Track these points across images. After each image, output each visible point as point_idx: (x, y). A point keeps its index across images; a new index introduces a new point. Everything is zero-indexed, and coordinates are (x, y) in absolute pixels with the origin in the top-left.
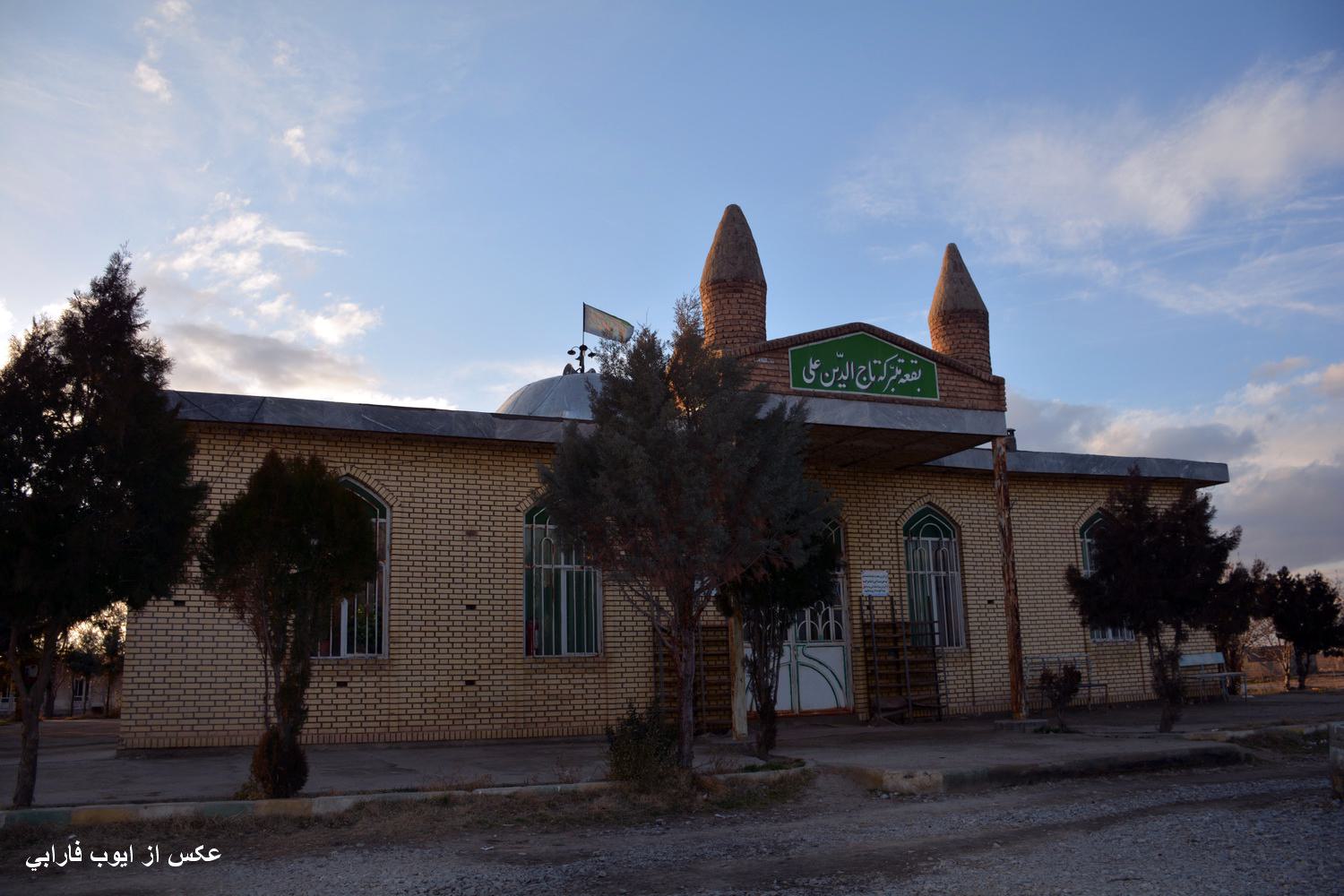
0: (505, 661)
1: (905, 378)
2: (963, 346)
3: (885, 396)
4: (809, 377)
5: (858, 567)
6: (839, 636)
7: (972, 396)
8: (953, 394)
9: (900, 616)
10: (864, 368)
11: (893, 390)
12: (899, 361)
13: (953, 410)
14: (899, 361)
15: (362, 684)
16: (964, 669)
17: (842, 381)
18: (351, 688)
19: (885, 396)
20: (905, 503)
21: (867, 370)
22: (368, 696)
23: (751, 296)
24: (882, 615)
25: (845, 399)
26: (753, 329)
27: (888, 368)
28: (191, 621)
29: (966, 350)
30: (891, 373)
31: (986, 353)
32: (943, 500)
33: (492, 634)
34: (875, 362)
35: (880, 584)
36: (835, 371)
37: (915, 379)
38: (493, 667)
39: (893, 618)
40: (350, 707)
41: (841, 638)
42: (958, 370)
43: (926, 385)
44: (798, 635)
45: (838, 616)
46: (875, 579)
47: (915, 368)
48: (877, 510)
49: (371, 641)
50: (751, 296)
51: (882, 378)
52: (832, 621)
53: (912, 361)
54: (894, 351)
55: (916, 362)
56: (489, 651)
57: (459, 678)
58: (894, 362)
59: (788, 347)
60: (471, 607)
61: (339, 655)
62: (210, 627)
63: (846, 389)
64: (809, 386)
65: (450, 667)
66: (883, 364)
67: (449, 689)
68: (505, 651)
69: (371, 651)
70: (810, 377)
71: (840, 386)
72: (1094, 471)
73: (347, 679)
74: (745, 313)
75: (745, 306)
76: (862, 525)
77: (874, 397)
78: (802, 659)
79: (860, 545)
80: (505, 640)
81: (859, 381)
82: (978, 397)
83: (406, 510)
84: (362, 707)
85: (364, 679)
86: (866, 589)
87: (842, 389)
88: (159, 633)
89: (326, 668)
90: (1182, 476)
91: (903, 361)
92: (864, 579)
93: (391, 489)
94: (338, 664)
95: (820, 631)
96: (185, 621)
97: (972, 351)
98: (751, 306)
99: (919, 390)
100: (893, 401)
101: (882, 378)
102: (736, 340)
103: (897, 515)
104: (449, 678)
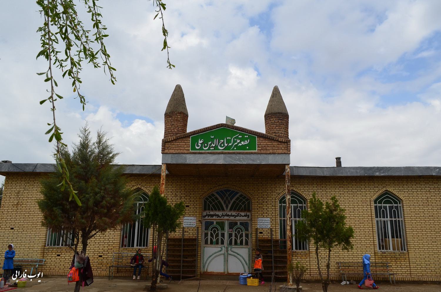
0: (113, 249)
1: (241, 143)
2: (271, 128)
3: (232, 151)
4: (198, 146)
5: (257, 216)
6: (247, 243)
7: (274, 148)
8: (265, 148)
9: (275, 237)
10: (223, 141)
11: (235, 148)
12: (239, 137)
13: (263, 155)
14: (239, 137)
15: (65, 256)
16: (306, 260)
17: (212, 147)
18: (61, 257)
19: (232, 151)
20: (280, 190)
21: (224, 142)
22: (66, 259)
23: (176, 118)
24: (266, 235)
25: (212, 154)
26: (176, 130)
27: (234, 140)
28: (15, 234)
29: (272, 130)
30: (234, 142)
31: (185, 129)
32: (299, 189)
33: (109, 240)
34: (228, 138)
35: (266, 224)
36: (209, 143)
37: (246, 143)
38: (108, 251)
39: (271, 237)
40: (60, 263)
41: (248, 245)
42: (267, 138)
43: (251, 146)
44: (229, 243)
45: (247, 236)
46: (263, 221)
47: (247, 139)
48: (266, 193)
49: (386, 245)
50: (176, 118)
51: (230, 144)
52: (244, 238)
53: (245, 136)
54: (237, 133)
55: (247, 137)
56: (108, 245)
57: (97, 254)
58: (237, 138)
59: (190, 136)
60: (12, 229)
61: (134, 247)
62: (20, 236)
63: (214, 150)
64: (198, 150)
65: (94, 251)
66: (231, 139)
67: (93, 258)
68: (113, 245)
69: (304, 249)
70: (198, 146)
71: (211, 149)
72: (377, 174)
73: (60, 254)
74: (173, 125)
75: (173, 122)
76: (259, 200)
77: (249, 152)
78: (230, 252)
79: (258, 207)
80: (113, 242)
81: (220, 146)
82: (276, 148)
83: (256, 200)
84: (64, 263)
85: (66, 254)
86: (259, 225)
87: (212, 150)
88: (5, 238)
89: (54, 250)
90: (434, 174)
91: (241, 137)
92: (258, 221)
93: (251, 193)
94: (58, 249)
95: (239, 241)
96: (13, 234)
97: (276, 129)
98: (175, 122)
99: (247, 148)
100: (234, 153)
101: (230, 144)
102: (169, 135)
103: (276, 195)
104: (93, 254)
